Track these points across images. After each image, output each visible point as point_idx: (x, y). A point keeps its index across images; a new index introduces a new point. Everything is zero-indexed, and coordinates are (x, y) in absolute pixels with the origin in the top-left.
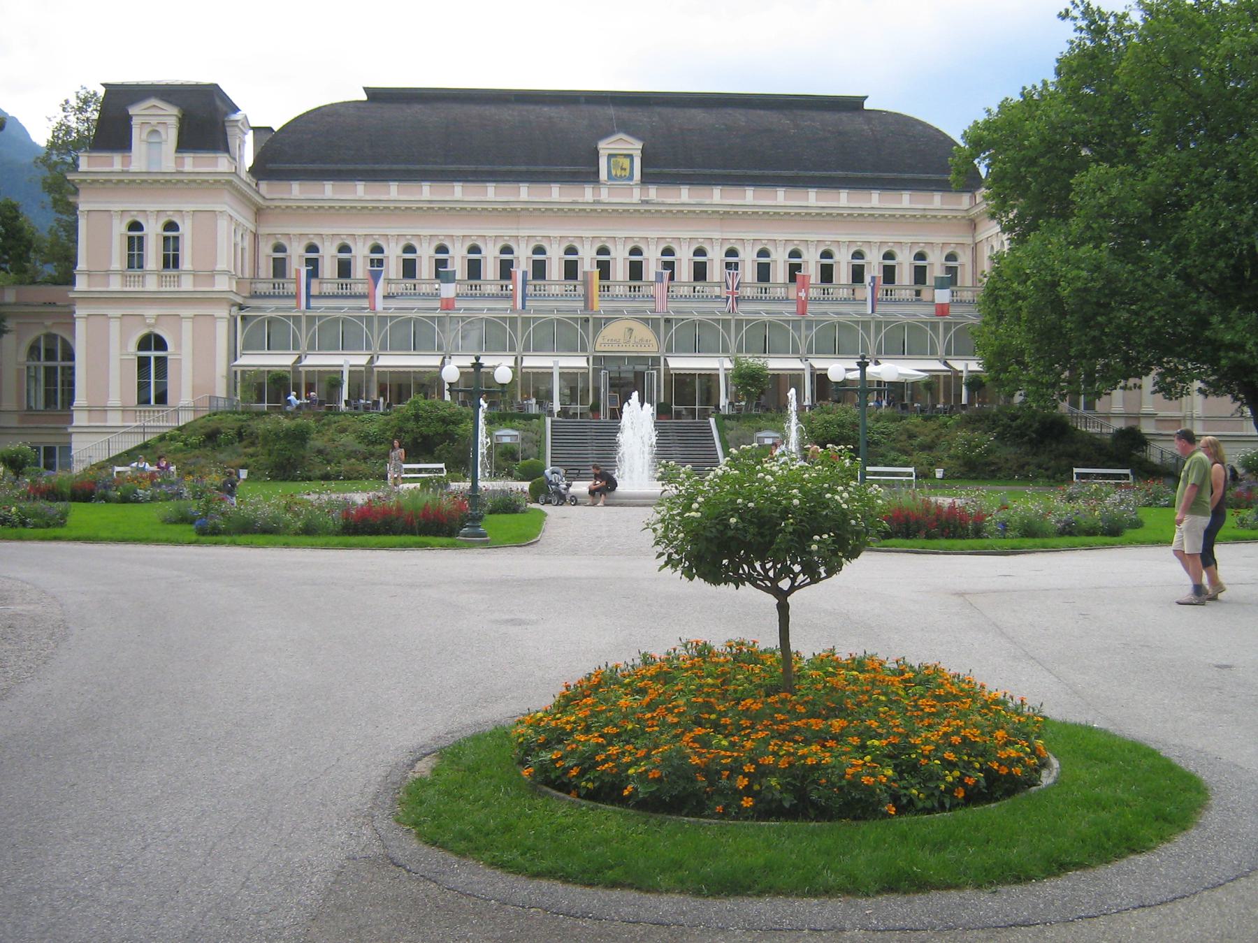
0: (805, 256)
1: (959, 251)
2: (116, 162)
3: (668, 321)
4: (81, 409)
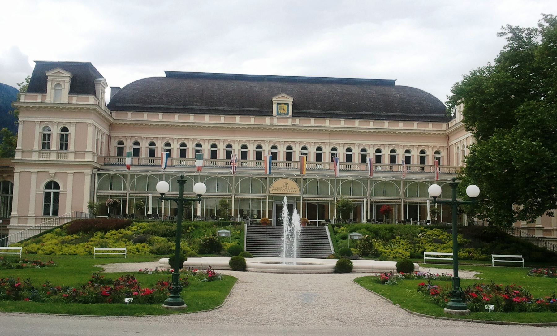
0: (339, 150)
1: (441, 150)
2: (39, 98)
3: (304, 179)
4: (14, 217)
